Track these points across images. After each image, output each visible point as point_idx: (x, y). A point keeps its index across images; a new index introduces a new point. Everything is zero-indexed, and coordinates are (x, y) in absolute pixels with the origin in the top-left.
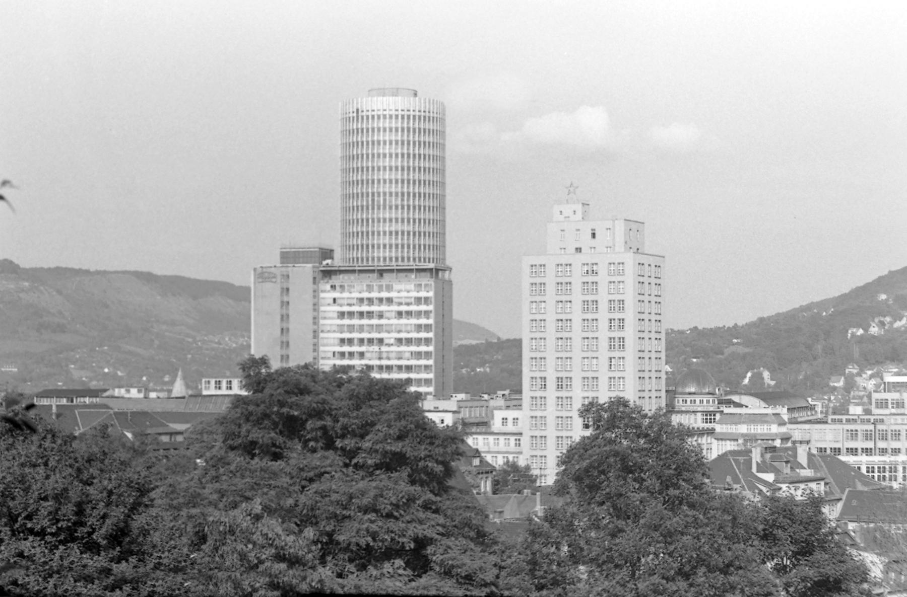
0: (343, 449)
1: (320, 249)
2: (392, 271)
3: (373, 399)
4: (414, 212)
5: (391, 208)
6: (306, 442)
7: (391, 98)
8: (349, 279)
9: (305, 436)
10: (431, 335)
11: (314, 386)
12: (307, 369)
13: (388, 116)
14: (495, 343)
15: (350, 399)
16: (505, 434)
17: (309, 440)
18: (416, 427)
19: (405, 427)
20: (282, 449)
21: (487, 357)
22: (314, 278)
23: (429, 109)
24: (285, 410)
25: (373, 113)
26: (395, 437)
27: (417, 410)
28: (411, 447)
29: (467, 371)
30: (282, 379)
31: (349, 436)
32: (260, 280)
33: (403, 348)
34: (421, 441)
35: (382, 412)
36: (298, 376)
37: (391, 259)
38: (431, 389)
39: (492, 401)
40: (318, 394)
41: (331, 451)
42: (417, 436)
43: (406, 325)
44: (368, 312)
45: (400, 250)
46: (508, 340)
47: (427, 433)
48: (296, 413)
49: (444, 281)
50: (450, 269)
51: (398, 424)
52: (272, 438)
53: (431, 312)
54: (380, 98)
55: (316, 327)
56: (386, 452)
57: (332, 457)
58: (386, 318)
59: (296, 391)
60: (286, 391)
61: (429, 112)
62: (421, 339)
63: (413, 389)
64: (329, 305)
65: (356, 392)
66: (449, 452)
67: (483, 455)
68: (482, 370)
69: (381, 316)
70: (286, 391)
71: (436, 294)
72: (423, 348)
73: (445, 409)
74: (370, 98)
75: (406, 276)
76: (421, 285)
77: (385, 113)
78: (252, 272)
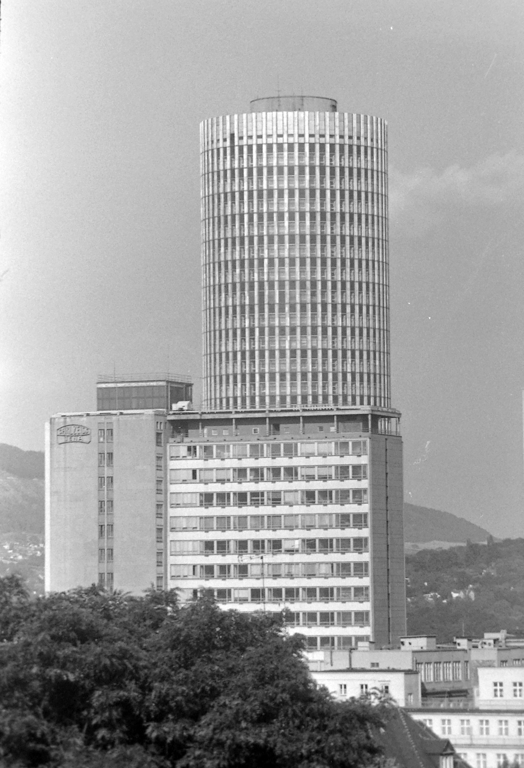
0: (160, 742)
1: (168, 382)
2: (295, 420)
3: (215, 647)
4: (334, 314)
5: (293, 308)
6: (92, 731)
7: (290, 114)
8: (220, 434)
9: (91, 720)
10: (365, 533)
11: (106, 626)
12: (97, 594)
13: (286, 146)
14: (484, 546)
15: (173, 648)
16: (498, 712)
17: (97, 727)
18: (292, 698)
19: (272, 699)
20: (47, 745)
21: (469, 571)
22: (158, 435)
23: (359, 132)
24: (53, 672)
25: (260, 141)
26: (255, 717)
27: (294, 665)
28: (284, 735)
29: (434, 597)
30: (48, 613)
31: (170, 716)
32: (62, 439)
33: (317, 557)
34: (302, 723)
35: (232, 671)
36: (76, 607)
37: (294, 399)
38: (367, 631)
39: (474, 652)
40: (113, 641)
41: (138, 747)
42: (295, 715)
43: (321, 515)
44: (254, 494)
45: (288, 383)
46: (508, 542)
47: (314, 706)
48: (72, 677)
49: (387, 435)
50: (399, 416)
51: (260, 692)
52: (28, 725)
53: (365, 491)
54: (272, 115)
55: (161, 522)
56: (239, 746)
57: (139, 759)
58: (286, 504)
59: (73, 635)
60: (53, 637)
61: (359, 138)
62: (348, 540)
63: (291, 631)
64: (184, 481)
65: (184, 634)
66: (355, 744)
67: (458, 751)
68: (461, 594)
69: (276, 500)
70: (53, 637)
71: (373, 461)
72: (352, 557)
73: (391, 667)
74: (254, 115)
75: (321, 429)
76: (347, 443)
77: (280, 140)
78: (47, 426)
